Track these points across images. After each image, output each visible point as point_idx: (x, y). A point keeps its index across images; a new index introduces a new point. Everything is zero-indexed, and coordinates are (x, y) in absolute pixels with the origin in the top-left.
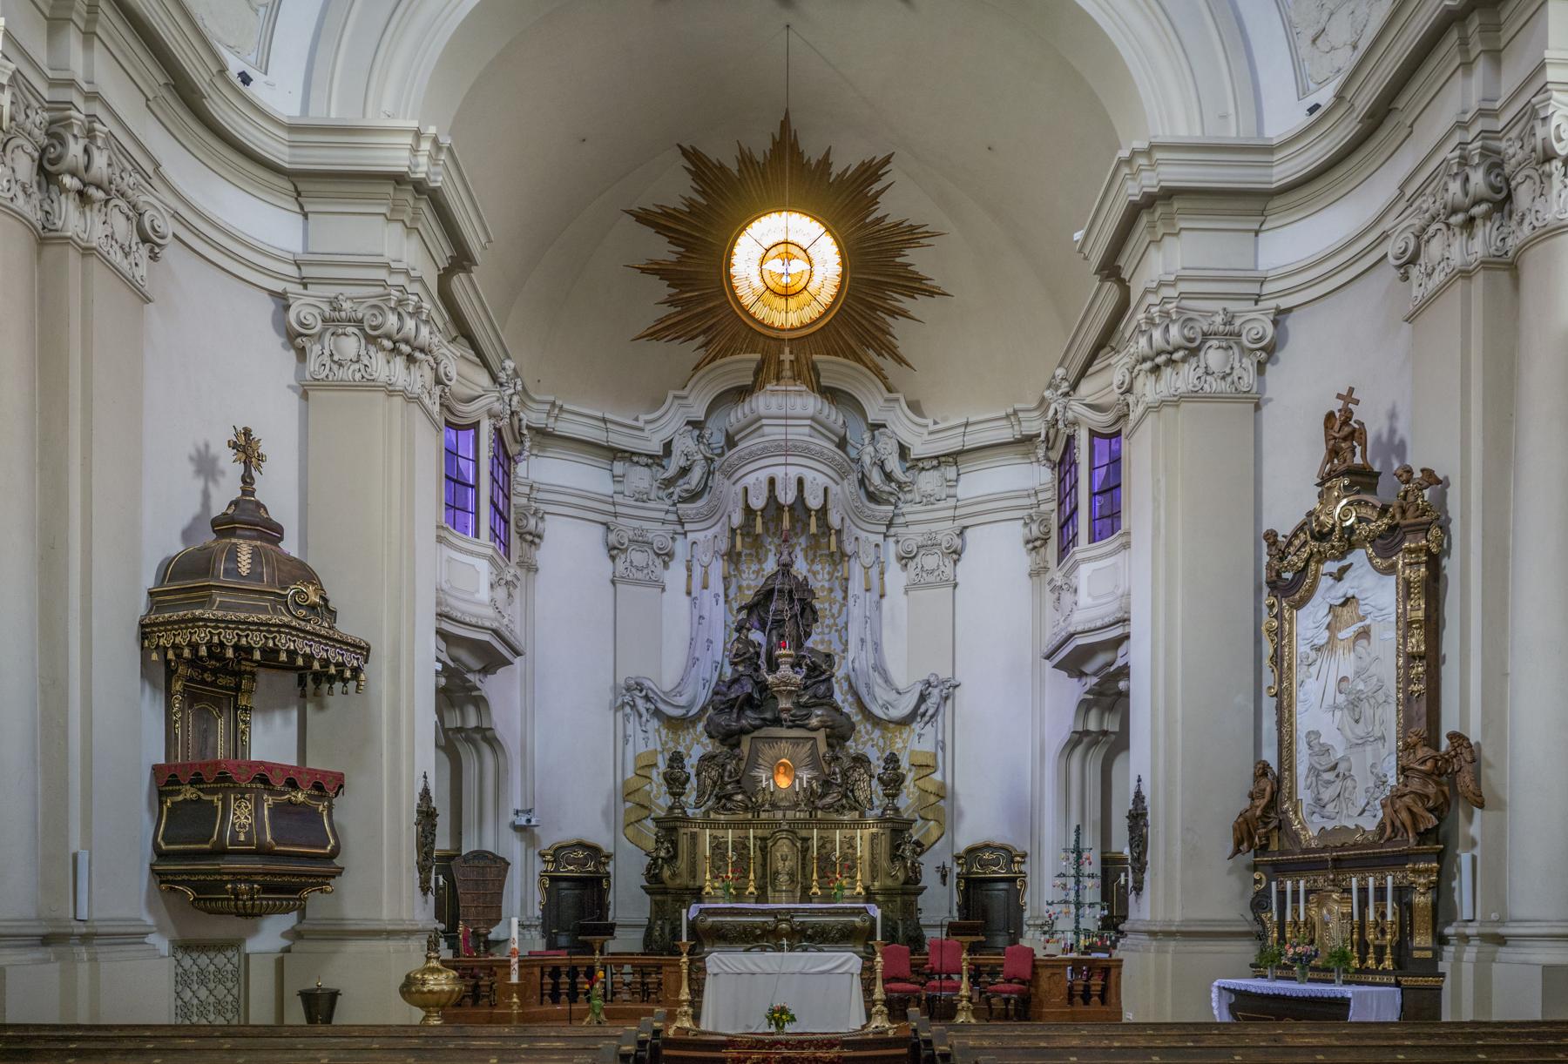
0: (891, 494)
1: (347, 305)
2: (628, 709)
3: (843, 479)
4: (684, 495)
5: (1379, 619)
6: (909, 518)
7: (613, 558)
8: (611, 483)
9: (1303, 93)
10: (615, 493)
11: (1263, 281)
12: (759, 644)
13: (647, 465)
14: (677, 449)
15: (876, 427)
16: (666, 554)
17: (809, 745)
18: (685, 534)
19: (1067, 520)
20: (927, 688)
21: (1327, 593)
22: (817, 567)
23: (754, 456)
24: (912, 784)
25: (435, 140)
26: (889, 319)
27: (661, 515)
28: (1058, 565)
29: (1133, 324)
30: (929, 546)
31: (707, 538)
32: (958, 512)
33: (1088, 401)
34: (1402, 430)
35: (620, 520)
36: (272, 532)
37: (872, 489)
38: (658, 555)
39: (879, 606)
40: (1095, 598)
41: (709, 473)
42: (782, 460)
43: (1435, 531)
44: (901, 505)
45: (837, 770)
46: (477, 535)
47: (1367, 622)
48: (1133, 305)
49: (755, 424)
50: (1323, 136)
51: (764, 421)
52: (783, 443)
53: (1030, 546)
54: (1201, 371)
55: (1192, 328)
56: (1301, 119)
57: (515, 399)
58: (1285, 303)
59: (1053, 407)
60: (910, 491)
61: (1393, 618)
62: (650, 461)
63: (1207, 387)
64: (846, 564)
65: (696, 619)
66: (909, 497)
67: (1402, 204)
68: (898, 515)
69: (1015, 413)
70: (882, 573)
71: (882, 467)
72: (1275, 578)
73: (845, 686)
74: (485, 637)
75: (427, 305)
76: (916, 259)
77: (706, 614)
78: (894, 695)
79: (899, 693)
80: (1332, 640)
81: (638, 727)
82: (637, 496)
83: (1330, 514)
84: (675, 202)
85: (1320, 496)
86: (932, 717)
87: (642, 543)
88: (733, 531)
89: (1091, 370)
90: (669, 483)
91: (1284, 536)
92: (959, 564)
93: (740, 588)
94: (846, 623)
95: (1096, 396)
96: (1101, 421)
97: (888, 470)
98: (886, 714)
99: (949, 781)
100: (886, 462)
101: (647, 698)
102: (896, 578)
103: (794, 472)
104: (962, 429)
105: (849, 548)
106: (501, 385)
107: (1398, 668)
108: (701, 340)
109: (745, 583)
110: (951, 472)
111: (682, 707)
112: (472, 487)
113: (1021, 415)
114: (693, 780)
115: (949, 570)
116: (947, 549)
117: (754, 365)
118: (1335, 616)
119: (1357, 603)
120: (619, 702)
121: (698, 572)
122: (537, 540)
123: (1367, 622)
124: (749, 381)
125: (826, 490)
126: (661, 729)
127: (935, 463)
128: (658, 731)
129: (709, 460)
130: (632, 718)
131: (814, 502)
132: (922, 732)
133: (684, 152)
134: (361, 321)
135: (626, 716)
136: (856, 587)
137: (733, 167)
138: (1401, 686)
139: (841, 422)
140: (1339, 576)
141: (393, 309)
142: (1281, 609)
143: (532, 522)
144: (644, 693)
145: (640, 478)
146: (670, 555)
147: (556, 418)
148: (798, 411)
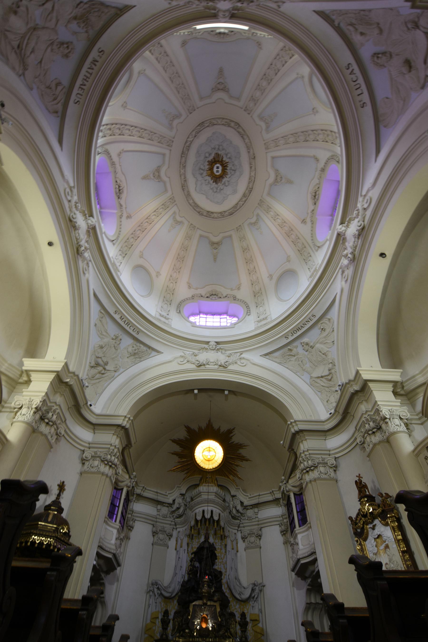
0: (239, 517)
1: (98, 453)
2: (151, 593)
3: (224, 511)
4: (177, 516)
5: (390, 541)
6: (245, 525)
7: (154, 536)
8: (156, 511)
9: (328, 412)
10: (157, 515)
11: (330, 451)
12: (197, 567)
13: (167, 507)
14: (176, 502)
15: (233, 496)
16: (170, 535)
17: (214, 608)
18: (177, 529)
19: (292, 522)
20: (254, 587)
21: (372, 535)
22: (217, 541)
23: (199, 503)
24: (251, 629)
25: (129, 418)
26: (236, 467)
27: (170, 522)
28: (291, 536)
29: (299, 461)
30: (251, 534)
31: (183, 530)
32: (259, 523)
33: (292, 485)
34: (377, 486)
35: (158, 524)
36: (60, 510)
37: (233, 515)
38: (167, 535)
39: (236, 554)
40: (304, 546)
41: (185, 510)
42: (207, 505)
43: (395, 511)
44: (242, 520)
45: (224, 619)
46: (115, 521)
47: (387, 542)
48: (298, 457)
49: (199, 494)
50: (334, 419)
51: (202, 494)
52: (207, 500)
53: (282, 533)
54: (319, 472)
55: (314, 461)
56: (328, 416)
57: (134, 483)
58: (337, 456)
59: (282, 487)
60: (245, 516)
61: (393, 540)
62: (168, 505)
63: (322, 477)
64: (226, 539)
65: (177, 558)
66: (244, 518)
67: (357, 431)
68: (241, 524)
69: (273, 492)
70: (237, 543)
71: (236, 508)
72: (356, 531)
73: (226, 586)
74: (110, 556)
75: (118, 454)
76: (243, 452)
77: (181, 557)
78: (243, 589)
79: (244, 588)
80: (378, 550)
81: (154, 600)
82: (163, 516)
83: (364, 509)
84: (182, 437)
85: (360, 504)
86: (257, 598)
87: (163, 531)
88: (191, 527)
89: (291, 477)
90: (173, 512)
91: (354, 518)
92: (261, 540)
93: (192, 548)
94: (226, 561)
95: (294, 483)
96: (296, 490)
97: (238, 509)
98: (241, 597)
99: (265, 628)
100: (237, 507)
101: (158, 588)
102: (241, 545)
103: (210, 508)
104: (258, 497)
105: (227, 534)
106: (131, 479)
107: (401, 557)
108: (186, 472)
109: (194, 546)
110: (256, 510)
111: (170, 593)
112: (117, 507)
113: (274, 492)
114: (171, 622)
115: (258, 542)
116: (257, 534)
117: (199, 479)
118: (377, 542)
119: (382, 537)
120: (149, 590)
121: (179, 541)
122: (131, 529)
123: (387, 542)
124: (198, 483)
125: (219, 514)
126: (162, 602)
127: (251, 507)
128: (161, 603)
129: (186, 505)
130: (152, 597)
131: (216, 518)
132: (254, 605)
133: (185, 427)
134: (101, 457)
135: (150, 596)
136: (229, 547)
137: (197, 430)
138: (404, 563)
139: (223, 494)
140: (373, 528)
141: (110, 454)
142: (360, 542)
143: (131, 522)
144: (157, 586)
145: (165, 510)
146: (171, 536)
147: (144, 491)
148: (212, 491)
